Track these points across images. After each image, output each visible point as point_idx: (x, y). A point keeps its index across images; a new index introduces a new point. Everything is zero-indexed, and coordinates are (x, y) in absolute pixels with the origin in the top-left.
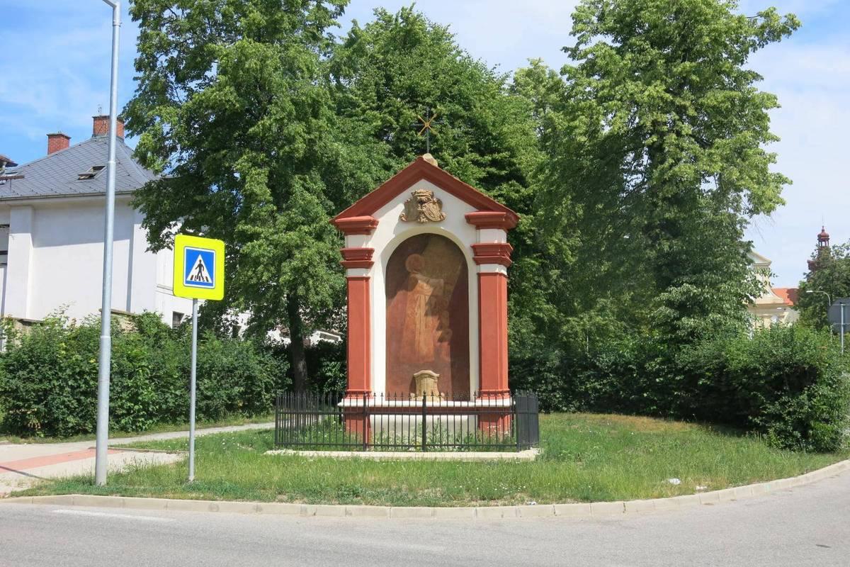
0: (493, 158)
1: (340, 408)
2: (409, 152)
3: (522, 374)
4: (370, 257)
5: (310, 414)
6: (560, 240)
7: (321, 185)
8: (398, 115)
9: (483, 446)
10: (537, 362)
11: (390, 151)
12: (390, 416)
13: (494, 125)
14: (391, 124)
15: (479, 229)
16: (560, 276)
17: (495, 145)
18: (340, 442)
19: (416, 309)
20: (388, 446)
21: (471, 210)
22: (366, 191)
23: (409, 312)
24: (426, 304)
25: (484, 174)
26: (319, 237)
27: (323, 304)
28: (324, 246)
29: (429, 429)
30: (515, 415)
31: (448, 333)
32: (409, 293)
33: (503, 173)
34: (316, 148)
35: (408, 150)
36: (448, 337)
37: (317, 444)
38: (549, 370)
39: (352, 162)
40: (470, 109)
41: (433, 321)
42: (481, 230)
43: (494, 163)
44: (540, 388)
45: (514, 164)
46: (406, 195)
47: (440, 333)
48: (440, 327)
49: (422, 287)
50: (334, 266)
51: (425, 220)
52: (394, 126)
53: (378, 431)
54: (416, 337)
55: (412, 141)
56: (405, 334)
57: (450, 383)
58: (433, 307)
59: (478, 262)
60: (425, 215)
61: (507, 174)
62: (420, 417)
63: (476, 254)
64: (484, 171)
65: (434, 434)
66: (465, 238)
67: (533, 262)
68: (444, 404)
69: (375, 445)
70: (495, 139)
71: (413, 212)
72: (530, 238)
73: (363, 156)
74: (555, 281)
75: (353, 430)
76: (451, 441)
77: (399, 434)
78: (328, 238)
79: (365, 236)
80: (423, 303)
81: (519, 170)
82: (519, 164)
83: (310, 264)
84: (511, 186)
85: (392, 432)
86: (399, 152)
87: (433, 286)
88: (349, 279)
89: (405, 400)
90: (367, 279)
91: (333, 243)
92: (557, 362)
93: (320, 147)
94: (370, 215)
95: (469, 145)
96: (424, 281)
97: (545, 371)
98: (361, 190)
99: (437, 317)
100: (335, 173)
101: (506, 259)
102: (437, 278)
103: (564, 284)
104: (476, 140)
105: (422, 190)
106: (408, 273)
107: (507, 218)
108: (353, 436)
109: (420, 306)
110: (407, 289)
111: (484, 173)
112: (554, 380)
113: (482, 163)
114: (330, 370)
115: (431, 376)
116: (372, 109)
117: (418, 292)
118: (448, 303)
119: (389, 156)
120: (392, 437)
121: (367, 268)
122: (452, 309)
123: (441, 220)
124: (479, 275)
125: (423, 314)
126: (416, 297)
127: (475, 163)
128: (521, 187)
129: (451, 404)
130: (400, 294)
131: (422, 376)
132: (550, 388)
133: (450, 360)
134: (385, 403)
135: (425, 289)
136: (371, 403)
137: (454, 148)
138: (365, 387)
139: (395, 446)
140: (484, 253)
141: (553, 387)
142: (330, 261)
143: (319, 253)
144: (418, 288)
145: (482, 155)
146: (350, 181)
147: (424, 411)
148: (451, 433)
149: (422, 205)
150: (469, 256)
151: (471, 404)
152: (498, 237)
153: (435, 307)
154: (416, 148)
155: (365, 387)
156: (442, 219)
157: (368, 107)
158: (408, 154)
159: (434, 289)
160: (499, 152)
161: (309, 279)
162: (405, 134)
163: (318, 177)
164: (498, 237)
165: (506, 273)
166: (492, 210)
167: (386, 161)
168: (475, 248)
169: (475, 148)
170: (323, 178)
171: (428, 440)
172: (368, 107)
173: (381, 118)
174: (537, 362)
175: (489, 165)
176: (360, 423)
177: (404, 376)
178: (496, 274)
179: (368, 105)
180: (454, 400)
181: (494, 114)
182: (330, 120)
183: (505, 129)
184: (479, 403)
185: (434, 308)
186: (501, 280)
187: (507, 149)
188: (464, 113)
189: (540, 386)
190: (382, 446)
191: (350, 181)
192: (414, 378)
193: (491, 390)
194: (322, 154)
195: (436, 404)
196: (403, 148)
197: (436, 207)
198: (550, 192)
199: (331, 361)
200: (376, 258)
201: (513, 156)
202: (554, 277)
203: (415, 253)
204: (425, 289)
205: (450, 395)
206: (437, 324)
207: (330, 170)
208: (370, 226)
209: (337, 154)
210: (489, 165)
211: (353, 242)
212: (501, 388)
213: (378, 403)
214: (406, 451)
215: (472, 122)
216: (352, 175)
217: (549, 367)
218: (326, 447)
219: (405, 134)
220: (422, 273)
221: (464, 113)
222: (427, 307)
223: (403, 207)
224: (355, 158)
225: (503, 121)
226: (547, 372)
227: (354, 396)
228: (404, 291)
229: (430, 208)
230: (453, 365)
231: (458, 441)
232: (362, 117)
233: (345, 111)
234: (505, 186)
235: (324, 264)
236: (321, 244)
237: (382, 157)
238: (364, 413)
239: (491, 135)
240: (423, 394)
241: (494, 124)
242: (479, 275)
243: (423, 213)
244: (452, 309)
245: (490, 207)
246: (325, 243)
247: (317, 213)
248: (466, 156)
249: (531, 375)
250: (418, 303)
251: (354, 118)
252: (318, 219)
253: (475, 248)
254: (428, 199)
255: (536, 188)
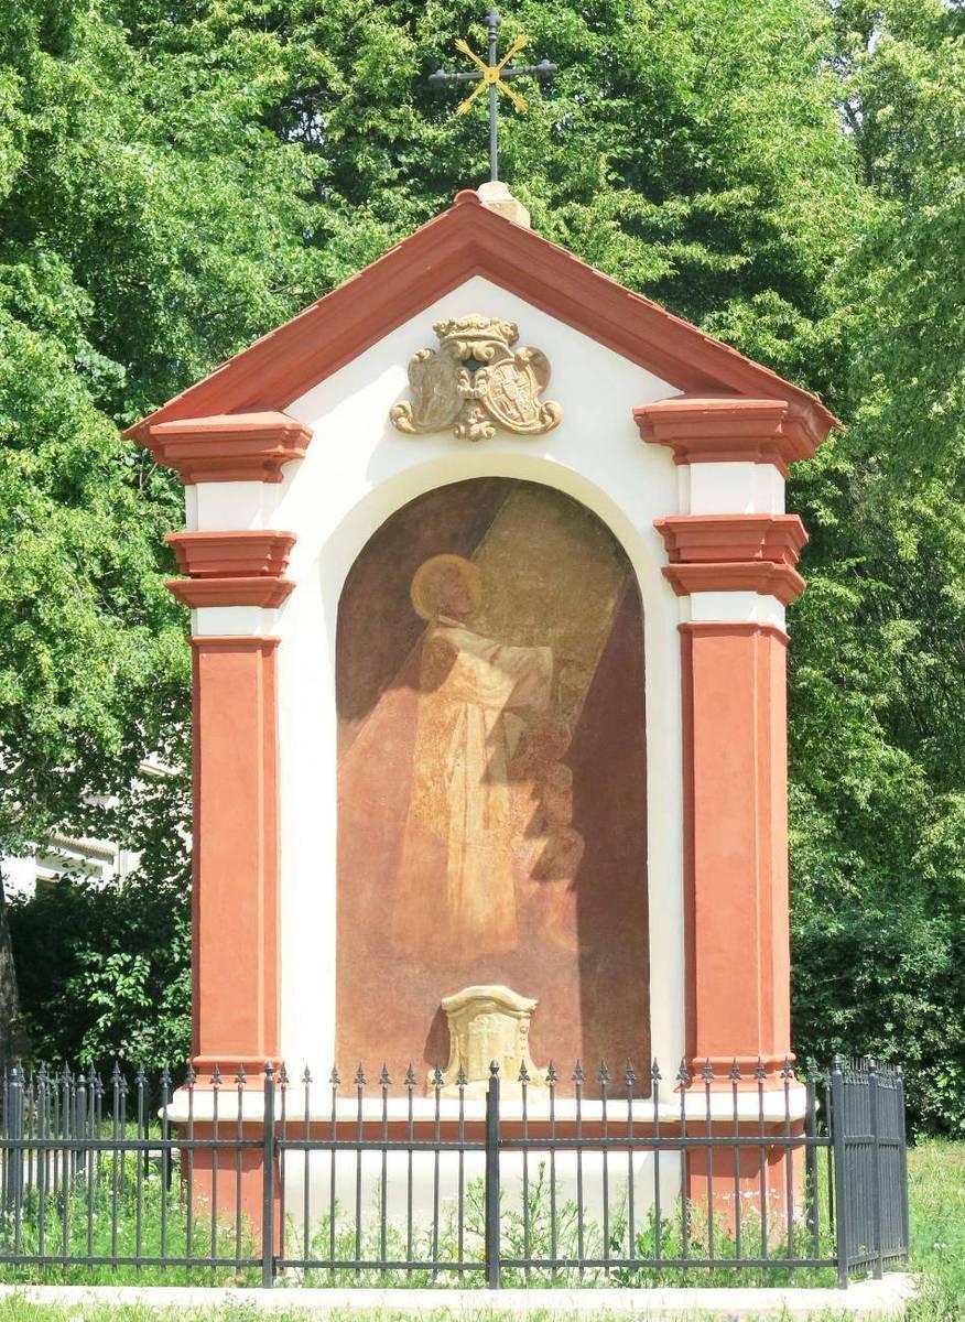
0: (695, 210)
1: (174, 1127)
2: (390, 184)
3: (836, 995)
4: (278, 564)
5: (65, 1147)
6: (939, 511)
7: (76, 302)
8: (349, 48)
9: (711, 1264)
10: (869, 955)
11: (321, 181)
12: (611, 1155)
13: (698, 89)
14: (323, 81)
15: (686, 462)
16: (918, 644)
17: (702, 159)
18: (177, 1250)
19: (450, 761)
20: (138, 1263)
21: (658, 393)
22: (239, 329)
23: (422, 769)
24: (488, 741)
25: (663, 268)
26: (70, 492)
27: (84, 739)
28: (90, 525)
29: (510, 1203)
30: (822, 1151)
31: (567, 849)
32: (425, 700)
33: (734, 262)
34: (58, 168)
35: (385, 176)
36: (570, 862)
37: (89, 1262)
38: (913, 986)
39: (188, 215)
40: (612, 29)
41: (512, 803)
42: (695, 467)
43: (699, 227)
44: (877, 1051)
45: (774, 232)
46: (415, 335)
47: (538, 847)
48: (541, 825)
49: (471, 679)
50: (121, 601)
51: (484, 427)
52: (333, 85)
53: (320, 1209)
54: (451, 867)
55: (401, 145)
56: (407, 850)
57: (578, 1031)
58: (512, 750)
59: (681, 584)
60: (485, 410)
61: (743, 268)
62: (476, 1161)
63: (675, 553)
64: (664, 257)
65: (526, 1224)
66: (637, 496)
67: (840, 591)
68: (566, 1110)
69: (307, 1265)
70: (703, 138)
71: (446, 392)
72: (832, 503)
73: (227, 191)
74: (902, 660)
75: (218, 1207)
76: (593, 1250)
77: (397, 1221)
78: (100, 495)
79: (259, 484)
80: (476, 736)
81: (787, 254)
82: (792, 232)
83: (45, 590)
84: (761, 310)
85: (371, 1214)
86: (349, 185)
87: (512, 675)
88: (198, 647)
89: (396, 1095)
90: (268, 647)
91: (119, 509)
92: (939, 956)
93: (72, 162)
94: (280, 410)
95: (611, 161)
96: (481, 654)
97: (895, 987)
98: (220, 326)
99: (530, 787)
100: (123, 257)
101: (787, 573)
102: (529, 642)
103: (933, 674)
104: (634, 143)
105: (476, 319)
106: (422, 625)
107: (790, 420)
108: (225, 1227)
109: (463, 745)
110: (415, 686)
111: (667, 264)
112: (930, 1019)
113: (656, 226)
114: (108, 987)
115: (504, 1007)
116: (250, 23)
117: (459, 696)
118: (570, 738)
119: (312, 197)
120: (370, 1233)
121: (268, 605)
122: (588, 762)
123: (545, 431)
124: (688, 633)
125: (476, 770)
126: (449, 713)
127: (632, 225)
128: (796, 313)
129: (592, 1110)
130: (391, 702)
131: (473, 1007)
132: (915, 1050)
133: (574, 949)
134: (347, 1111)
135: (483, 681)
136: (292, 1107)
137: (556, 172)
138: (261, 1047)
139: (384, 1266)
140: (699, 552)
141: (925, 1045)
142: (110, 579)
143: (71, 550)
144: (456, 681)
145: (656, 196)
146: (179, 280)
147: (493, 1136)
148: (593, 1216)
149: (473, 371)
150: (648, 561)
151: (669, 1110)
152: (749, 491)
153: (520, 752)
154: (416, 170)
155: (261, 1047)
156: (549, 421)
157: (236, 17)
158: (386, 193)
159: (517, 686)
160: (718, 186)
161: (40, 646)
162: (374, 120)
163: (66, 271)
164: (749, 491)
165: (782, 627)
166: (734, 393)
167: (308, 214)
168: (673, 534)
169: (630, 172)
170: (78, 279)
171: (505, 1246)
172: (236, 17)
173: (284, 57)
174: (869, 955)
175: (680, 234)
176: (254, 1178)
177: (405, 997)
178: (747, 629)
179: (239, 9)
180: (602, 1095)
181: (698, 48)
182: (107, 60)
183: (740, 103)
184: (696, 1106)
185: (519, 755)
186: (767, 650)
187: (747, 176)
188: (594, 42)
189: (877, 1042)
190: (332, 1265)
191: (179, 280)
192: (442, 1014)
193: (741, 1059)
194: (79, 188)
195: (539, 1110)
196: (367, 169)
197: (528, 378)
198: (910, 332)
199: (108, 953)
200: (298, 567)
201: (767, 201)
202: (898, 647)
203: (449, 549)
204: (483, 681)
205: (566, 1075)
206: (527, 812)
207: (106, 243)
208: (281, 449)
209: (136, 191)
210: (680, 234)
211: (217, 508)
212: (771, 1052)
213: (320, 1112)
214: (423, 1284)
215: (620, 77)
216: (189, 264)
217: (911, 974)
218: (123, 1269)
219: (374, 120)
220: (470, 626)
221: (594, 42)
222: (491, 751)
223: (404, 381)
224: (199, 201)
225: (735, 72)
226: (904, 991)
227: (228, 1082)
228: (405, 692)
229: (503, 383)
230: (586, 964)
231: (616, 1247)
232: (214, 56)
233: (150, 32)
234: (738, 309)
235: (91, 592)
236: (77, 518)
237: (293, 200)
238: (261, 1145)
239: (689, 122)
240: (488, 1073)
241: (701, 79)
242: (688, 633)
243: (479, 401)
244: (588, 762)
245: (723, 377)
246: (94, 512)
247: (62, 402)
248: (600, 199)
249: (845, 1003)
250: (456, 735)
251: (187, 57)
252: (64, 426)
253: (673, 534)
254: (499, 349)
255: (852, 321)
